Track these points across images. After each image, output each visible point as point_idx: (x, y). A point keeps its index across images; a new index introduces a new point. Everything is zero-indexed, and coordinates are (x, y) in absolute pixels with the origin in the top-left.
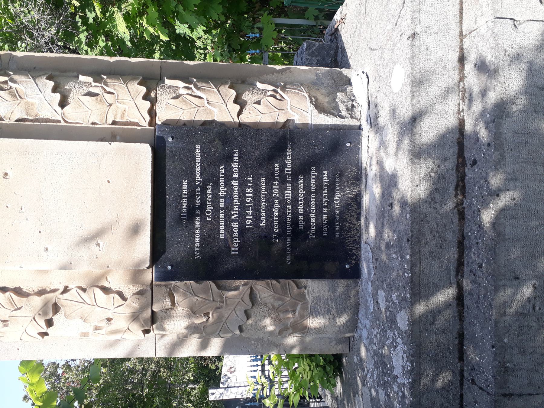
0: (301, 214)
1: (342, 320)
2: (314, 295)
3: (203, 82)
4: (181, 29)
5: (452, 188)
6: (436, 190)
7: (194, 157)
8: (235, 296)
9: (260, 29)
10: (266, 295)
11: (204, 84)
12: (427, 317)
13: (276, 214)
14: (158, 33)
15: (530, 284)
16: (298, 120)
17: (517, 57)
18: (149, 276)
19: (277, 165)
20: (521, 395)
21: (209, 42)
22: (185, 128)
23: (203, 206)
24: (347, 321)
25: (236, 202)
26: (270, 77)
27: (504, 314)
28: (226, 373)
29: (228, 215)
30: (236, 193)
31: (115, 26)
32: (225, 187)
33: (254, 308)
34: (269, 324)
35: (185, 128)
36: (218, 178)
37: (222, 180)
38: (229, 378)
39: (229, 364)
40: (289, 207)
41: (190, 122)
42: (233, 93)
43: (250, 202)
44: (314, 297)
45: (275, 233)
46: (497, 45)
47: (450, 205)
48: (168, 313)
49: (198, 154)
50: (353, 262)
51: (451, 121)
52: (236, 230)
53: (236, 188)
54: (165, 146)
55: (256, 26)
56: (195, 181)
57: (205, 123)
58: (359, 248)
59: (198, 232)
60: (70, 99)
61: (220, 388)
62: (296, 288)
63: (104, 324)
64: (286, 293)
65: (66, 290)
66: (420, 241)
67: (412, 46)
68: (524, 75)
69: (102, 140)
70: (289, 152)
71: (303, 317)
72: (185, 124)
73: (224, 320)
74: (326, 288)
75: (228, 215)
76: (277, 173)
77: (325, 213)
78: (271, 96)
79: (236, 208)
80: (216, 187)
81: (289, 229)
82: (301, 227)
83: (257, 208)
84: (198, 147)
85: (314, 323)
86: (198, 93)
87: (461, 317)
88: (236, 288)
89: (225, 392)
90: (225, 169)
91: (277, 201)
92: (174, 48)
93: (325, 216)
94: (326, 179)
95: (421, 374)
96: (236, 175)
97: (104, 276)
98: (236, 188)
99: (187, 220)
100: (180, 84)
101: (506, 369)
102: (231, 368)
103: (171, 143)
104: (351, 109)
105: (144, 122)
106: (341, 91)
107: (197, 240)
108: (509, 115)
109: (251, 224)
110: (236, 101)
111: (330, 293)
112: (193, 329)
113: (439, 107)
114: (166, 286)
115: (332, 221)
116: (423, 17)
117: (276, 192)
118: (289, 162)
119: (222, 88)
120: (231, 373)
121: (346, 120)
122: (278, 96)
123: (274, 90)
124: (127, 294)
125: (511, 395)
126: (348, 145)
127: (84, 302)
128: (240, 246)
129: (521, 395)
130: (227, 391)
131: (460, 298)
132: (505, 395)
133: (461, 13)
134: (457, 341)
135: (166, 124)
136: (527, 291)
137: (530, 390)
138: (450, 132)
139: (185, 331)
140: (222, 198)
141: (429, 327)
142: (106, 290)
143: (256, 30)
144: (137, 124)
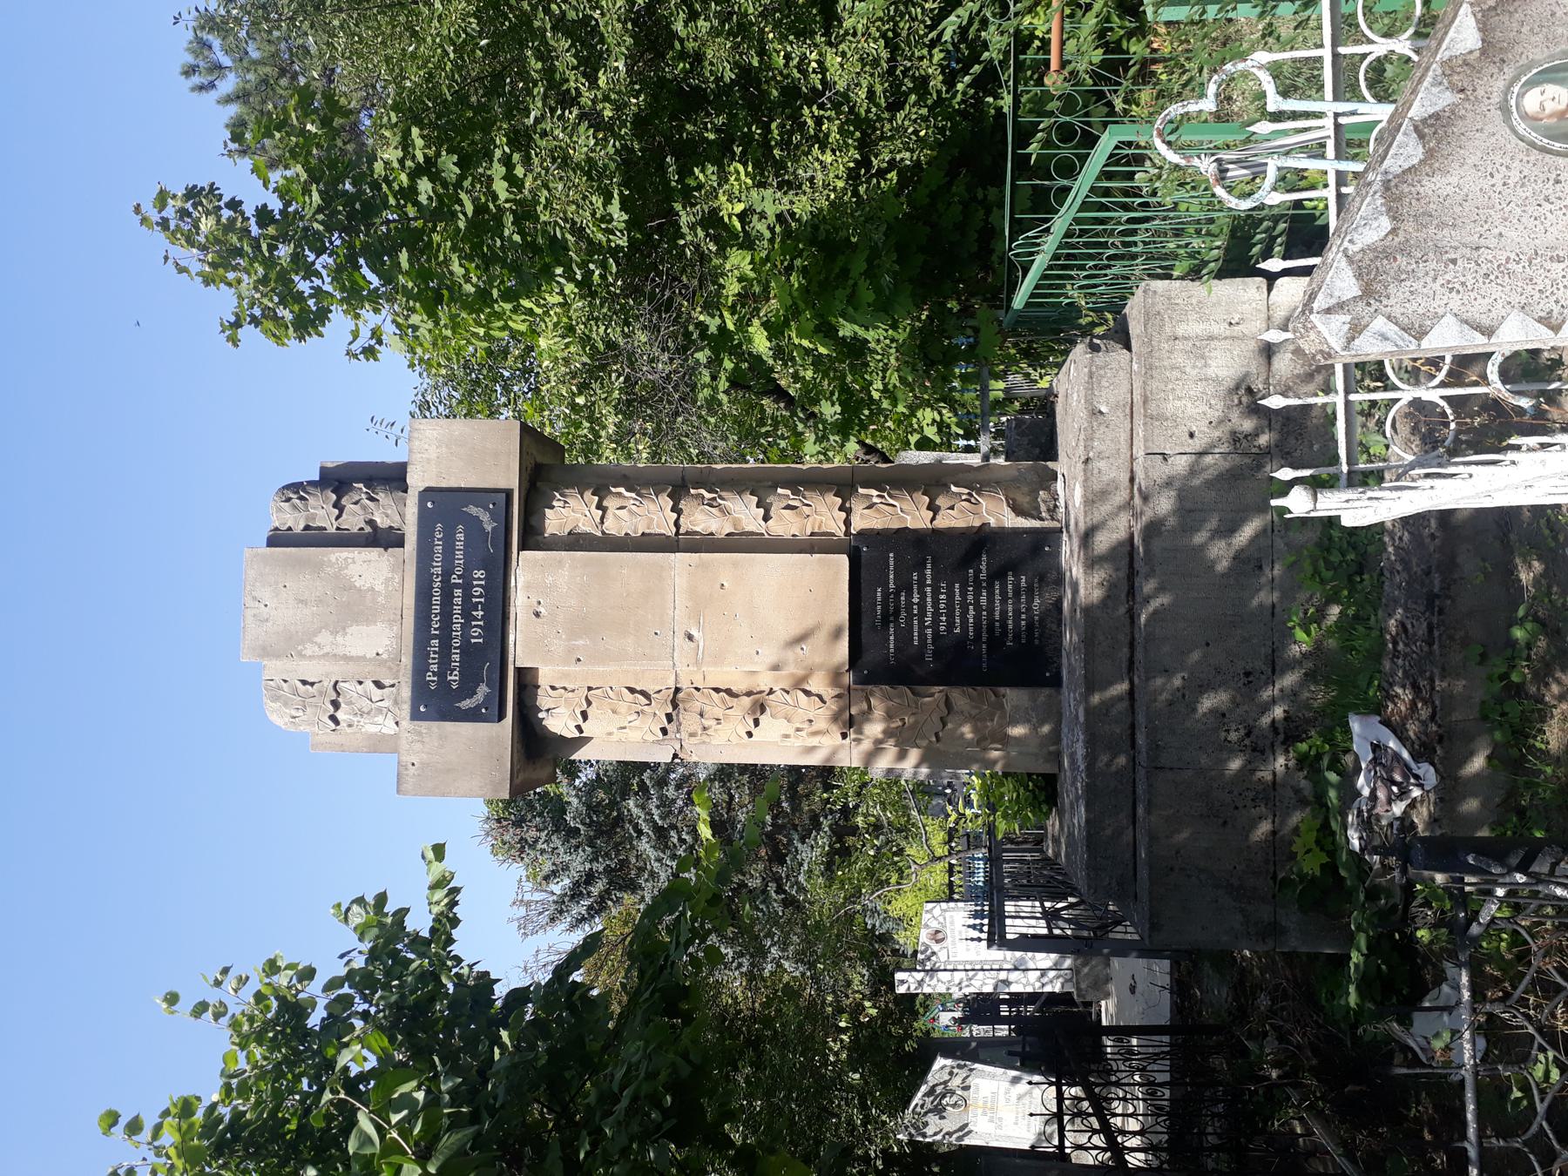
1: (1046, 729)
4: (846, 330)
5: (1123, 596)
6: (1109, 596)
9: (976, 330)
15: (1179, 676)
17: (1168, 484)
18: (848, 679)
23: (897, 613)
27: (1155, 700)
28: (928, 942)
29: (922, 622)
30: (929, 599)
31: (750, 340)
34: (967, 731)
37: (915, 587)
39: (934, 925)
42: (927, 499)
47: (1122, 610)
48: (867, 715)
53: (929, 594)
57: (898, 530)
59: (892, 638)
60: (772, 514)
63: (806, 725)
65: (771, 692)
67: (1085, 470)
68: (1172, 501)
69: (800, 552)
70: (984, 558)
71: (1003, 726)
75: (922, 622)
76: (971, 579)
79: (929, 614)
80: (910, 595)
81: (985, 636)
82: (997, 634)
83: (950, 615)
85: (1017, 731)
86: (891, 501)
87: (1132, 706)
88: (932, 695)
89: (927, 979)
93: (1023, 623)
94: (1023, 584)
96: (929, 582)
97: (804, 679)
98: (929, 594)
100: (874, 492)
102: (937, 932)
104: (1053, 510)
105: (840, 531)
107: (892, 646)
108: (1160, 533)
110: (929, 508)
112: (888, 733)
113: (1110, 523)
114: (862, 690)
115: (1030, 626)
117: (970, 598)
118: (983, 567)
120: (938, 941)
123: (969, 494)
124: (825, 698)
127: (787, 704)
128: (934, 653)
130: (932, 978)
131: (1131, 693)
132: (1156, 768)
135: (862, 534)
136: (1177, 682)
138: (1120, 544)
139: (880, 736)
142: (807, 693)
144: (833, 535)
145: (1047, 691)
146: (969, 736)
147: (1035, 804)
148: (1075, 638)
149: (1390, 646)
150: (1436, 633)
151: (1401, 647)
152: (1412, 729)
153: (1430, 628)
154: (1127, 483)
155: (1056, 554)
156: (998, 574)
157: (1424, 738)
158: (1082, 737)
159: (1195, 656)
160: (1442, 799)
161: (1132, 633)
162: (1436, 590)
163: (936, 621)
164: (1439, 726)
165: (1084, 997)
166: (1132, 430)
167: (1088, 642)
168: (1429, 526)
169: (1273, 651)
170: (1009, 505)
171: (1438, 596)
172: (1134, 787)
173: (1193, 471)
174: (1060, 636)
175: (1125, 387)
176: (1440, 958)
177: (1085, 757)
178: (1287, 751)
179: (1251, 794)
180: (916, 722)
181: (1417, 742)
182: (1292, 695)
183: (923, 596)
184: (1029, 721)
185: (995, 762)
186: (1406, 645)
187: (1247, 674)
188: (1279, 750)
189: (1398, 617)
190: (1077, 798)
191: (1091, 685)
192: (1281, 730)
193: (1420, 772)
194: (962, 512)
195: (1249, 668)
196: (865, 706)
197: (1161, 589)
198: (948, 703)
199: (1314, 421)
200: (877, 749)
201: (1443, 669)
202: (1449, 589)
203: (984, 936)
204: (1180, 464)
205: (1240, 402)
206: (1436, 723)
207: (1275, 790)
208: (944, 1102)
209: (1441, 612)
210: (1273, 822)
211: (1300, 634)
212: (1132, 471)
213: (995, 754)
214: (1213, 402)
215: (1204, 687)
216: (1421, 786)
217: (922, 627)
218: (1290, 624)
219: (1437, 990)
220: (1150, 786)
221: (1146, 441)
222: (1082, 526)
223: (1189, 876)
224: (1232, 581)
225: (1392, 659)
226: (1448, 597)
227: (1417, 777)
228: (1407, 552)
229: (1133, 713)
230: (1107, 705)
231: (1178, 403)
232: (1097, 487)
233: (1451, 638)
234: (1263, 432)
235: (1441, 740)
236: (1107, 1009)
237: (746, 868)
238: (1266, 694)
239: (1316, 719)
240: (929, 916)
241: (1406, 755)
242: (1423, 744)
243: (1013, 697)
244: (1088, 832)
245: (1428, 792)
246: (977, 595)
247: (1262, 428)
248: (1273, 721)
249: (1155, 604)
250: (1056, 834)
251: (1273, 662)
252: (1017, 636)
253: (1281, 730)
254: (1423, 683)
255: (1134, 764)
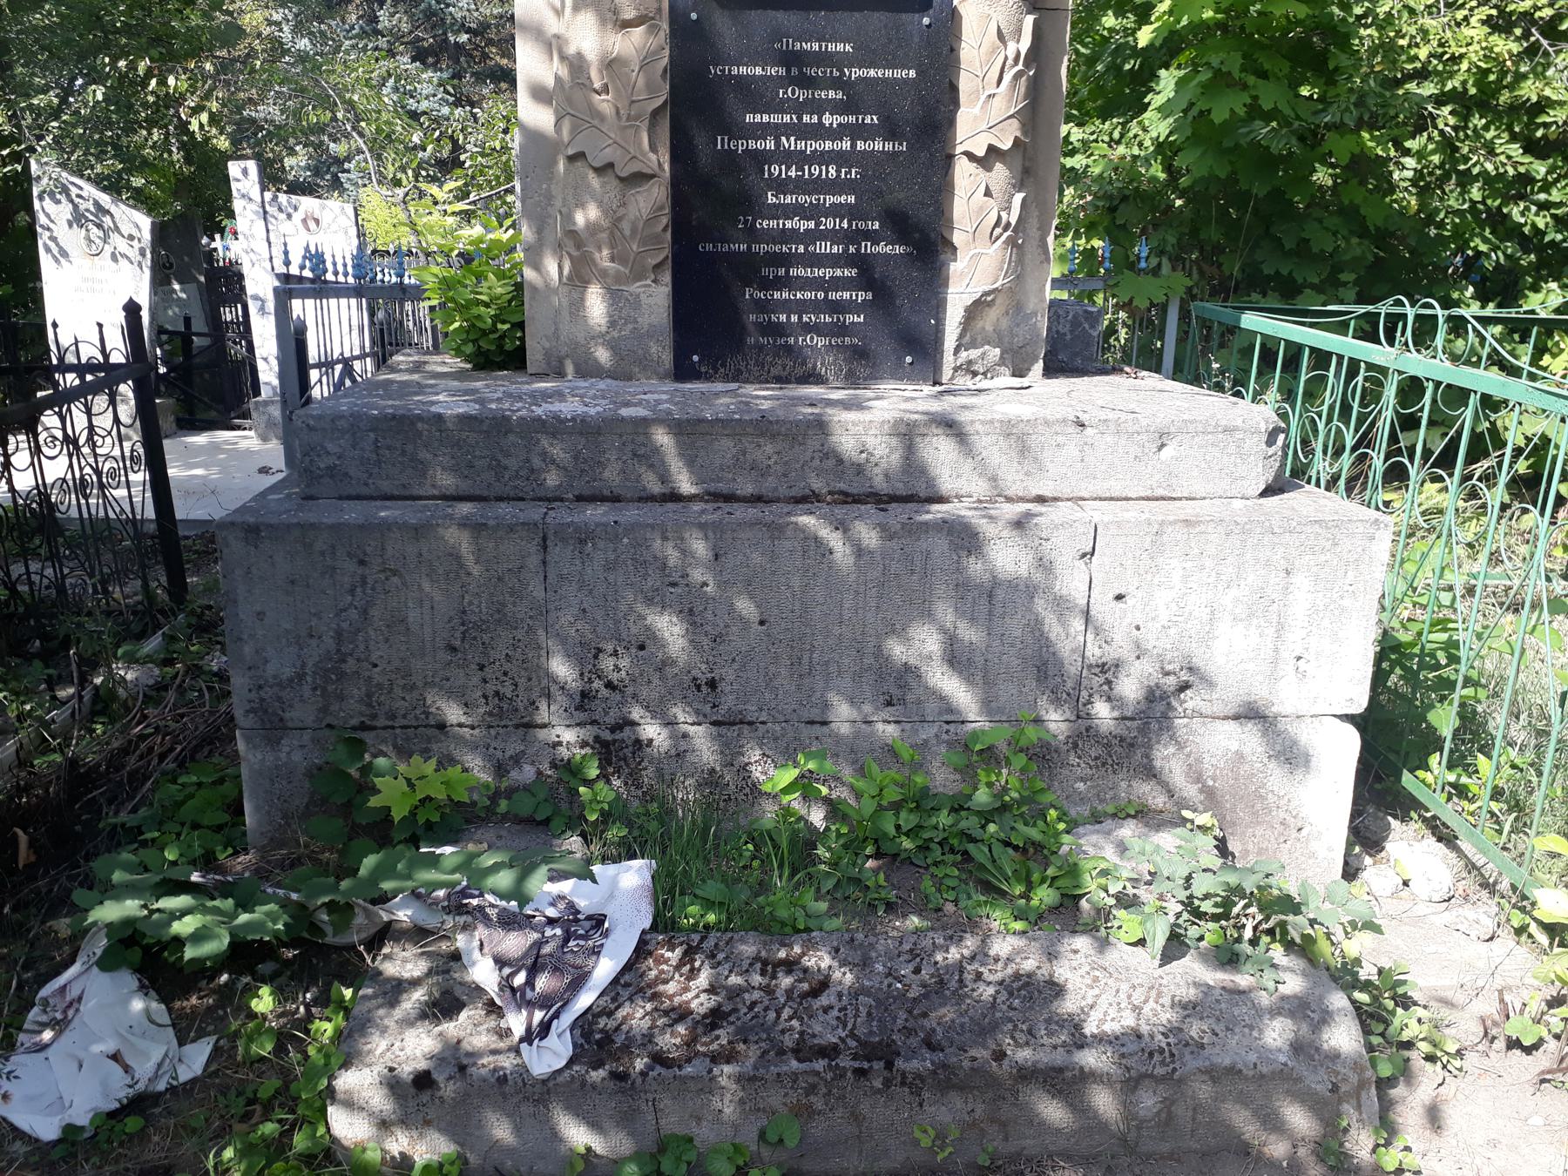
0: (787, 272)
1: (603, 355)
2: (643, 297)
3: (1028, 88)
5: (842, 486)
6: (840, 461)
7: (893, 67)
8: (640, 144)
9: (1156, 271)
10: (642, 204)
11: (1023, 90)
12: (644, 445)
13: (789, 225)
14: (1158, 19)
16: (956, 268)
17: (1044, 565)
19: (877, 226)
20: (544, 562)
21: (1136, 151)
22: (945, 51)
24: (596, 360)
25: (812, 146)
26: (1033, 223)
29: (788, 130)
30: (828, 145)
32: (840, 125)
33: (615, 182)
35: (945, 51)
36: (856, 113)
37: (852, 119)
38: (289, 216)
39: (326, 218)
40: (801, 249)
41: (958, 60)
42: (1006, 145)
43: (811, 174)
44: (638, 296)
45: (755, 221)
46: (1056, 527)
47: (817, 484)
49: (899, 74)
50: (703, 370)
51: (946, 485)
52: (760, 145)
53: (837, 146)
54: (914, 11)
55: (1165, 261)
56: (850, 66)
57: (954, 89)
58: (727, 379)
59: (758, 71)
61: (263, 189)
62: (654, 262)
64: (644, 244)
66: (762, 435)
70: (899, 249)
72: (952, 50)
73: (596, 122)
74: (655, 320)
75: (788, 130)
77: (789, 318)
78: (999, 218)
79: (801, 145)
80: (839, 108)
82: (765, 271)
83: (800, 186)
84: (912, 74)
85: (596, 306)
86: (1008, 77)
87: (651, 498)
88: (653, 148)
90: (872, 125)
91: (812, 225)
92: (1127, 67)
93: (783, 318)
95: (554, 436)
96: (860, 145)
98: (837, 146)
99: (780, 50)
100: (1025, 43)
101: (583, 542)
102: (317, 221)
103: (920, 22)
104: (969, 369)
106: (1002, 357)
107: (743, 70)
109: (770, 174)
110: (992, 149)
111: (646, 327)
112: (577, 65)
113: (968, 465)
114: (659, 10)
115: (778, 330)
116: (1109, 439)
117: (829, 223)
118: (883, 248)
119: (1015, 123)
120: (304, 221)
121: (952, 358)
122: (998, 231)
123: (1008, 224)
125: (545, 548)
126: (909, 359)
129: (544, 562)
131: (674, 497)
132: (544, 539)
133: (1112, 499)
134: (606, 493)
137: (552, 577)
138: (931, 482)
139: (571, 50)
140: (820, 119)
141: (630, 448)
143: (1154, 261)
145: (667, 358)
146: (580, 219)
147: (474, 332)
148: (766, 405)
149: (782, 954)
150: (820, 1065)
151: (786, 981)
152: (637, 1016)
153: (829, 1052)
154: (1035, 492)
155: (899, 374)
156: (868, 273)
157: (619, 1039)
158: (592, 411)
159: (745, 607)
160: (503, 1080)
161: (778, 500)
162: (900, 1063)
163: (788, 157)
164: (643, 1074)
165: (256, 409)
166: (1127, 499)
167: (764, 426)
168: (1018, 1045)
169: (751, 723)
170: (986, 294)
171: (889, 1065)
172: (508, 499)
173: (1062, 605)
174: (763, 380)
175: (1199, 489)
176: (220, 1031)
177: (556, 417)
178: (584, 744)
179: (507, 690)
180: (601, 117)
181: (612, 1024)
182: (680, 753)
183: (835, 134)
184: (612, 324)
185: (537, 267)
186: (789, 992)
187: (712, 684)
188: (587, 733)
189: (837, 975)
190: (482, 402)
191: (689, 430)
192: (618, 736)
193: (552, 1040)
194: (981, 208)
195: (722, 686)
196: (629, 14)
197: (859, 551)
198: (640, 178)
199: (1123, 784)
200: (552, 45)
201: (752, 1079)
202: (903, 1084)
203: (294, 270)
204: (1072, 582)
205: (1167, 674)
206: (650, 1068)
207: (517, 726)
208: (91, 226)
209: (861, 1073)
210: (460, 725)
211: (788, 776)
212: (1056, 499)
213: (551, 266)
214: (1172, 631)
215: (690, 616)
216: (528, 1038)
217: (777, 131)
218: (801, 758)
219: (166, 1020)
220: (511, 529)
221: (1119, 524)
222: (964, 417)
223: (352, 591)
224: (869, 660)
225: (757, 958)
226: (887, 1083)
227: (545, 1028)
228: (959, 997)
229: (640, 499)
230: (651, 457)
231: (1176, 577)
232: (1033, 441)
233: (811, 1090)
234: (1113, 708)
235: (619, 1077)
236: (245, 437)
237: (401, 8)
238: (681, 714)
239: (638, 787)
240: (338, 211)
241: (585, 1000)
242: (608, 1037)
243: (656, 298)
244: (419, 418)
245: (518, 1052)
246: (833, 236)
247: (1120, 707)
248: (634, 724)
249: (835, 540)
250: (428, 368)
251: (733, 724)
252: (763, 307)
253: (618, 736)
254: (724, 1035)
255: (549, 500)
